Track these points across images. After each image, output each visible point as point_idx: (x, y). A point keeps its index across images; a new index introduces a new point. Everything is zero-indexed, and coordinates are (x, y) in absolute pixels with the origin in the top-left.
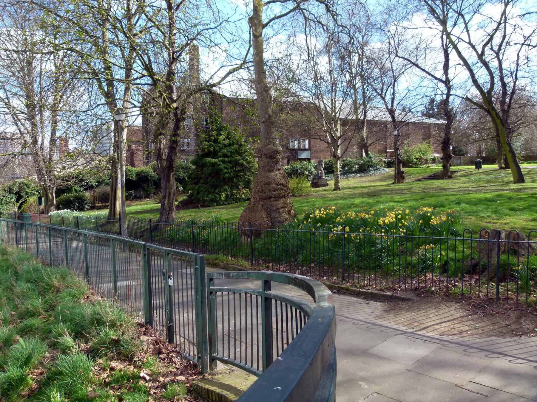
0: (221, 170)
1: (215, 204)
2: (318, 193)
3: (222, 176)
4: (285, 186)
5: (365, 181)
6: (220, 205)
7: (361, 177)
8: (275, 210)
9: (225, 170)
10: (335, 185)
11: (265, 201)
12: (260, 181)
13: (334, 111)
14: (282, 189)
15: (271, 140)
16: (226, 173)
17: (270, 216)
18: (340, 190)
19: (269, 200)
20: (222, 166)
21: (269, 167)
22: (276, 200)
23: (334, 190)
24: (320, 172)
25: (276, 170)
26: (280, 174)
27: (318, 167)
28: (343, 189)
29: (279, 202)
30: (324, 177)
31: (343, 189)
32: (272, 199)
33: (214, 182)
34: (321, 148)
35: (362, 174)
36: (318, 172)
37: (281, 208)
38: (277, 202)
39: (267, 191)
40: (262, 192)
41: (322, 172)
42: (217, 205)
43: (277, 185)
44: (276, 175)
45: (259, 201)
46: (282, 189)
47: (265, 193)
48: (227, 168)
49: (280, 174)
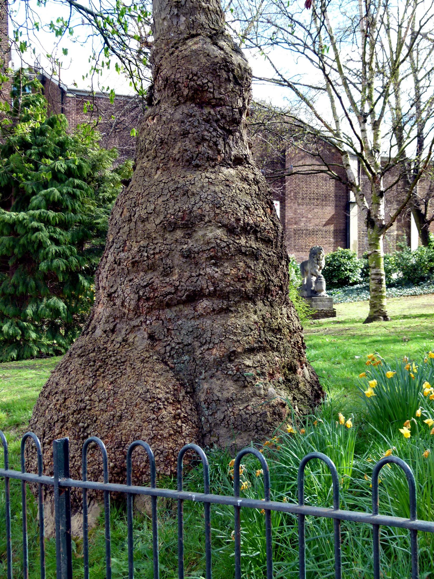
0: (41, 245)
1: (14, 355)
2: (325, 326)
3: (43, 266)
4: (267, 241)
5: (425, 306)
6: (32, 357)
7: (415, 295)
8: (219, 363)
9: (53, 248)
10: (373, 306)
11: (169, 313)
12: (141, 212)
13: (369, 98)
14: (255, 255)
15: (202, 18)
16: (58, 255)
17: (192, 393)
18: (386, 318)
19: (187, 310)
20: (44, 235)
21: (188, 144)
22: (227, 310)
23: (369, 320)
24: (314, 278)
25: (224, 163)
26: (245, 179)
27: (308, 267)
28: (396, 318)
29: (242, 322)
30: (324, 293)
31: (392, 319)
32: (204, 304)
33: (15, 286)
34: (311, 227)
35: (417, 289)
36: (309, 281)
37: (251, 351)
38: (232, 320)
39: (177, 260)
40: (152, 268)
41: (318, 281)
42: (19, 358)
43: (231, 230)
44: (227, 183)
45: (137, 312)
46: (255, 255)
47: (167, 272)
48: (57, 242)
49: (245, 179)
